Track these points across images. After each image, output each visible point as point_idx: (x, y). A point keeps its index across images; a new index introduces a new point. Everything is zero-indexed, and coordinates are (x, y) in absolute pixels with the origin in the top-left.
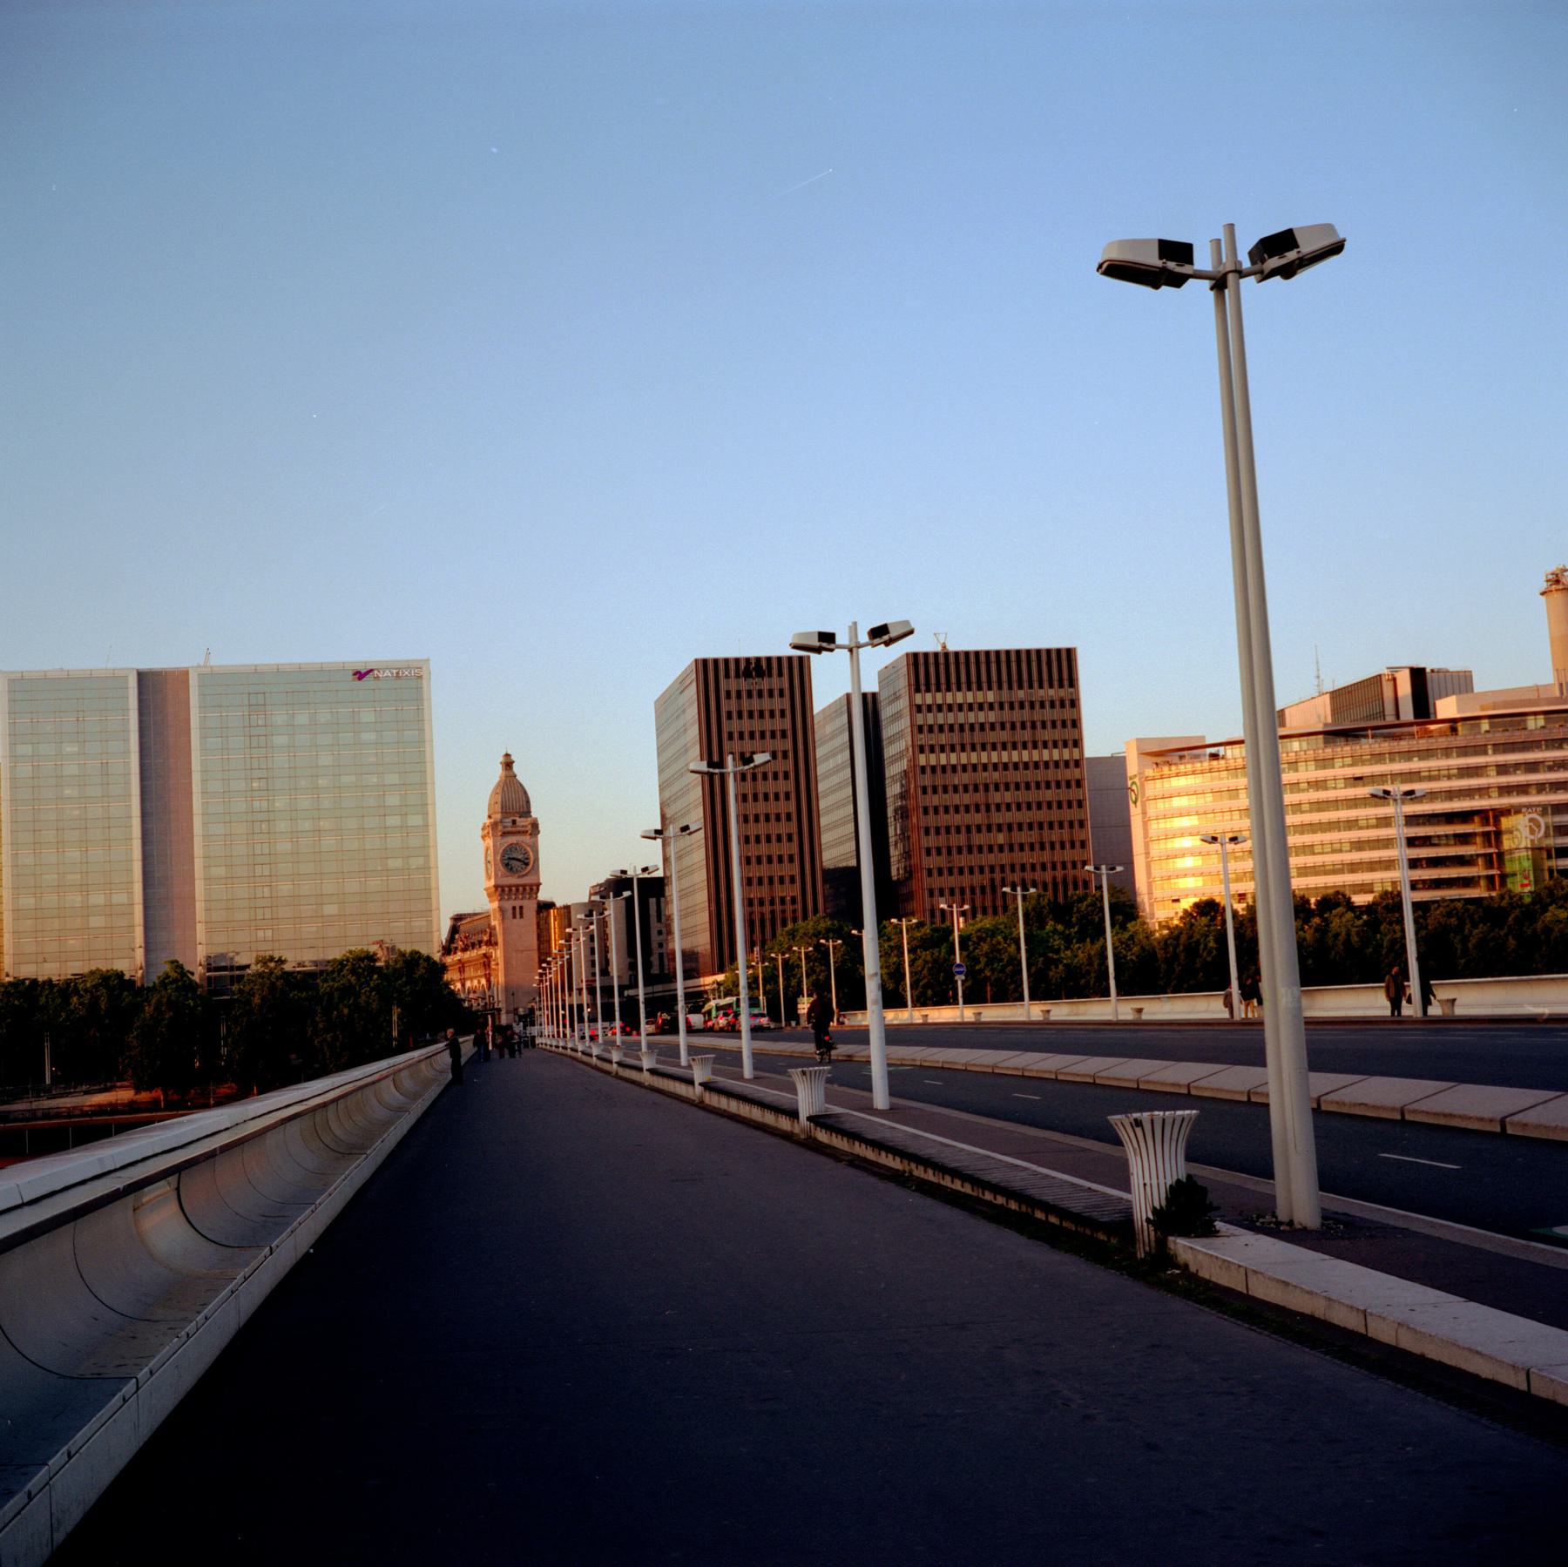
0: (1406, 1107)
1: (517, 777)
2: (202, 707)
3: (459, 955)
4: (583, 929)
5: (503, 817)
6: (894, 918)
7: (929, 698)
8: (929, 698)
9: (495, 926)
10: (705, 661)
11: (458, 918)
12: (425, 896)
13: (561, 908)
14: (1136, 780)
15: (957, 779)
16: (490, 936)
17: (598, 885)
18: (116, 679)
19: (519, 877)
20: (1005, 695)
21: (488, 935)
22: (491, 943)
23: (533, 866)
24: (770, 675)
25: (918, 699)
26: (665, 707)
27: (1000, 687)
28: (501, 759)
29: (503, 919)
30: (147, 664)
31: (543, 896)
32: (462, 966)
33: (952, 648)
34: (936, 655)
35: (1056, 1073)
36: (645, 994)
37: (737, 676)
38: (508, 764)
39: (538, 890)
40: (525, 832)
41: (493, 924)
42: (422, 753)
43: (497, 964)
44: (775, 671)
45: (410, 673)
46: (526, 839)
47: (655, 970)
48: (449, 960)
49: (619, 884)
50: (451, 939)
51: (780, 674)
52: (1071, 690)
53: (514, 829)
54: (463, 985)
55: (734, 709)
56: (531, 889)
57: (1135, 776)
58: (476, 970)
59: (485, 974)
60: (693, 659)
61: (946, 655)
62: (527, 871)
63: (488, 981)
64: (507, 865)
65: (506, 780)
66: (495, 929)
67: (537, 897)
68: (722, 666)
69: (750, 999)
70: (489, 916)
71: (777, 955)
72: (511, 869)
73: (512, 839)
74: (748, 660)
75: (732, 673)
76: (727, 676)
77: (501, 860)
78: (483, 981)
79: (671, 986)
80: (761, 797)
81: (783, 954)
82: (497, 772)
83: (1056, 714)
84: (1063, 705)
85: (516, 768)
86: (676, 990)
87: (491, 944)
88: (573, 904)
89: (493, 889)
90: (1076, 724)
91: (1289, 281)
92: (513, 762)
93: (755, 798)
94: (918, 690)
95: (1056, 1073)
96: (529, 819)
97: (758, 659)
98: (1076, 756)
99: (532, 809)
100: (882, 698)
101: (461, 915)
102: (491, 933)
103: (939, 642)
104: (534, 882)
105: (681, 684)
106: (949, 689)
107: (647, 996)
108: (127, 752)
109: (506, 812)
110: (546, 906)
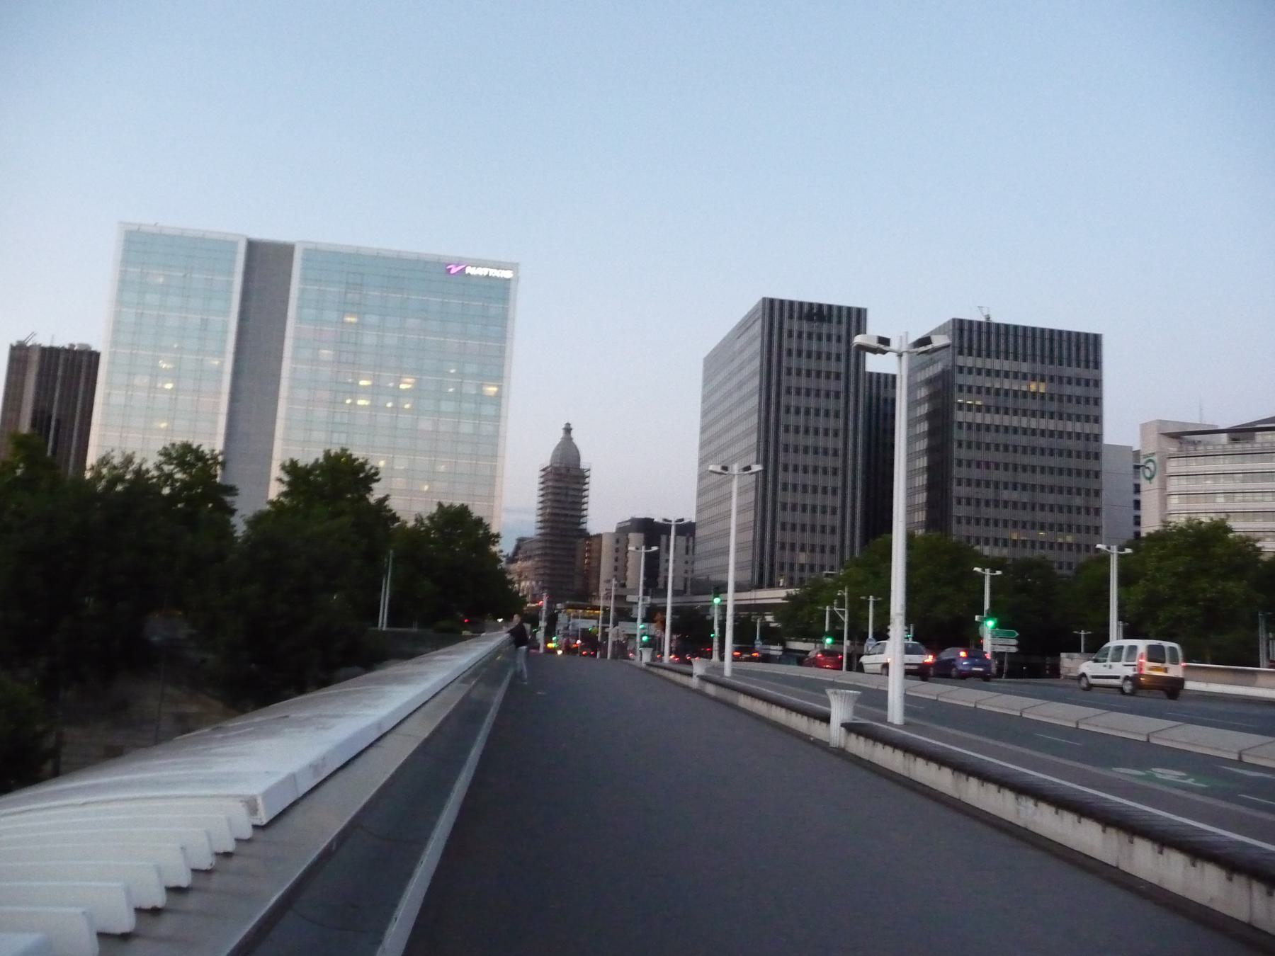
2: (304, 279)
10: (772, 301)
14: (1155, 458)
15: (988, 438)
18: (229, 245)
20: (1038, 368)
24: (830, 321)
26: (715, 363)
27: (1034, 360)
33: (996, 319)
34: (980, 323)
35: (938, 695)
36: (673, 603)
37: (800, 318)
38: (568, 430)
42: (502, 351)
44: (835, 319)
50: (515, 553)
51: (839, 322)
52: (1095, 372)
55: (794, 346)
57: (1153, 454)
61: (989, 324)
68: (786, 308)
71: (984, 570)
74: (811, 305)
75: (796, 315)
76: (791, 317)
80: (812, 431)
81: (993, 570)
82: (560, 434)
83: (1078, 391)
84: (1087, 384)
85: (573, 434)
90: (1098, 401)
91: (648, 516)
92: (571, 429)
93: (807, 431)
94: (961, 353)
95: (938, 695)
97: (820, 306)
98: (1096, 432)
101: (523, 538)
103: (983, 314)
105: (744, 326)
106: (989, 356)
107: (675, 605)
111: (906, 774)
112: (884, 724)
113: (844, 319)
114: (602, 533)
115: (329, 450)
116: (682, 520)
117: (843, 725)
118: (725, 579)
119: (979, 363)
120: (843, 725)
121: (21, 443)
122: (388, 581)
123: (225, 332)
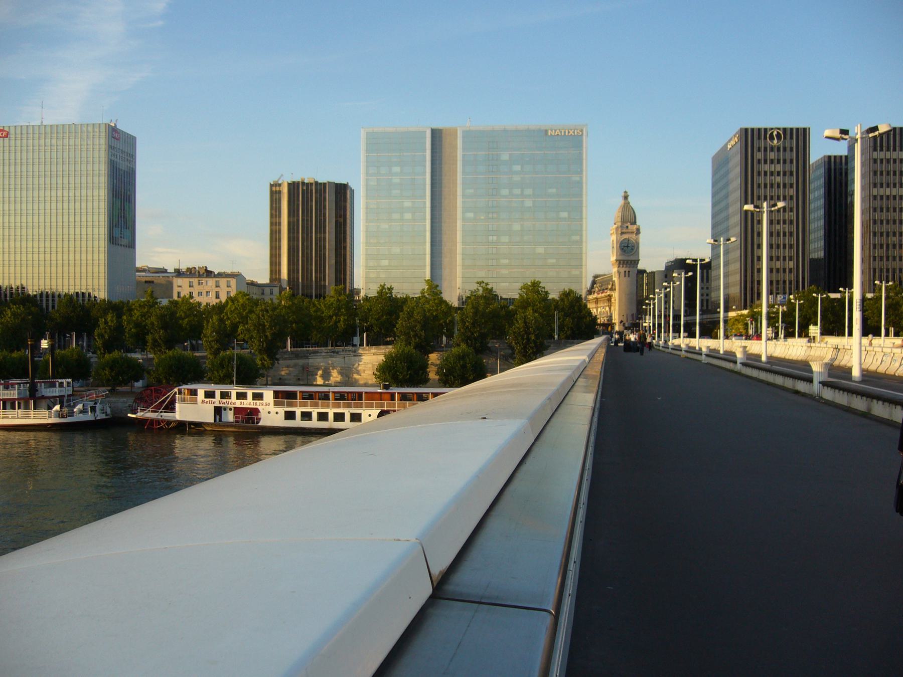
0: (808, 358)
1: (630, 204)
3: (595, 295)
4: (724, 241)
5: (622, 224)
6: (842, 287)
7: (882, 155)
8: (882, 155)
9: (614, 281)
10: (746, 130)
11: (596, 277)
12: (577, 259)
13: (650, 273)
16: (612, 286)
17: (670, 262)
19: (628, 256)
21: (611, 285)
22: (613, 289)
23: (636, 251)
25: (875, 155)
28: (623, 194)
29: (619, 277)
30: (435, 126)
31: (641, 266)
32: (597, 301)
38: (626, 197)
39: (638, 263)
40: (632, 233)
41: (614, 279)
43: (615, 300)
45: (574, 132)
46: (634, 236)
47: (705, 308)
48: (590, 297)
49: (681, 264)
50: (592, 287)
51: (791, 138)
53: (627, 231)
54: (597, 310)
56: (635, 262)
58: (604, 303)
59: (609, 305)
60: (739, 128)
62: (633, 252)
63: (610, 309)
64: (623, 249)
65: (624, 205)
66: (615, 282)
67: (637, 267)
68: (756, 133)
69: (42, 301)
70: (612, 276)
72: (625, 251)
73: (626, 236)
75: (762, 137)
76: (759, 138)
77: (620, 247)
78: (607, 309)
79: (716, 316)
82: (621, 202)
85: (629, 199)
86: (720, 318)
87: (613, 290)
88: (657, 271)
89: (615, 262)
92: (628, 196)
94: (875, 150)
96: (635, 226)
99: (637, 220)
100: (849, 157)
102: (612, 284)
104: (637, 259)
108: (425, 173)
109: (623, 221)
110: (643, 272)
111: (766, 380)
112: (849, 381)
113: (794, 137)
114: (654, 271)
115: (540, 283)
116: (875, 129)
117: (820, 383)
118: (679, 314)
119: (888, 155)
120: (820, 383)
121: (427, 281)
122: (857, 384)
123: (425, 185)
